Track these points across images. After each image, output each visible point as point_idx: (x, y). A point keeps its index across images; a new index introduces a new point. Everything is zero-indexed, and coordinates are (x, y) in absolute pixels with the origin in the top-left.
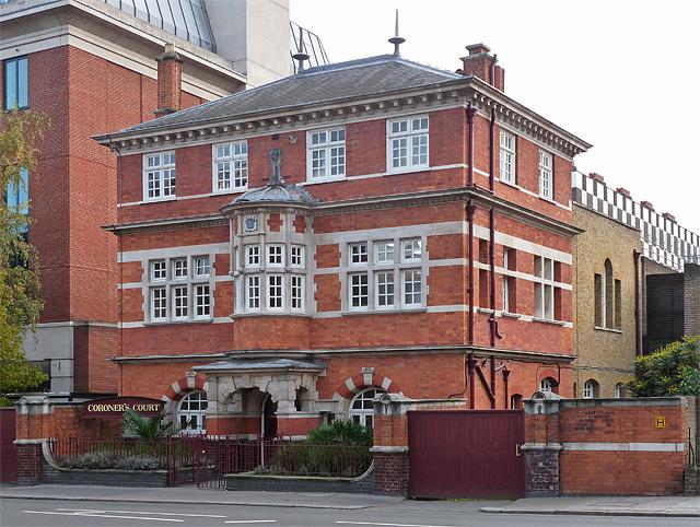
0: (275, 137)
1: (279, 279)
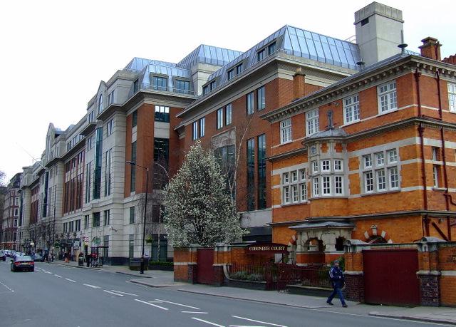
0: (330, 104)
1: (328, 178)
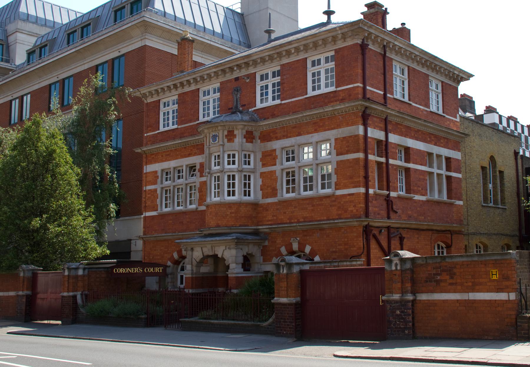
0: (237, 79)
